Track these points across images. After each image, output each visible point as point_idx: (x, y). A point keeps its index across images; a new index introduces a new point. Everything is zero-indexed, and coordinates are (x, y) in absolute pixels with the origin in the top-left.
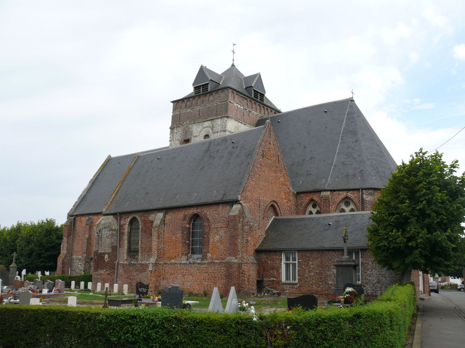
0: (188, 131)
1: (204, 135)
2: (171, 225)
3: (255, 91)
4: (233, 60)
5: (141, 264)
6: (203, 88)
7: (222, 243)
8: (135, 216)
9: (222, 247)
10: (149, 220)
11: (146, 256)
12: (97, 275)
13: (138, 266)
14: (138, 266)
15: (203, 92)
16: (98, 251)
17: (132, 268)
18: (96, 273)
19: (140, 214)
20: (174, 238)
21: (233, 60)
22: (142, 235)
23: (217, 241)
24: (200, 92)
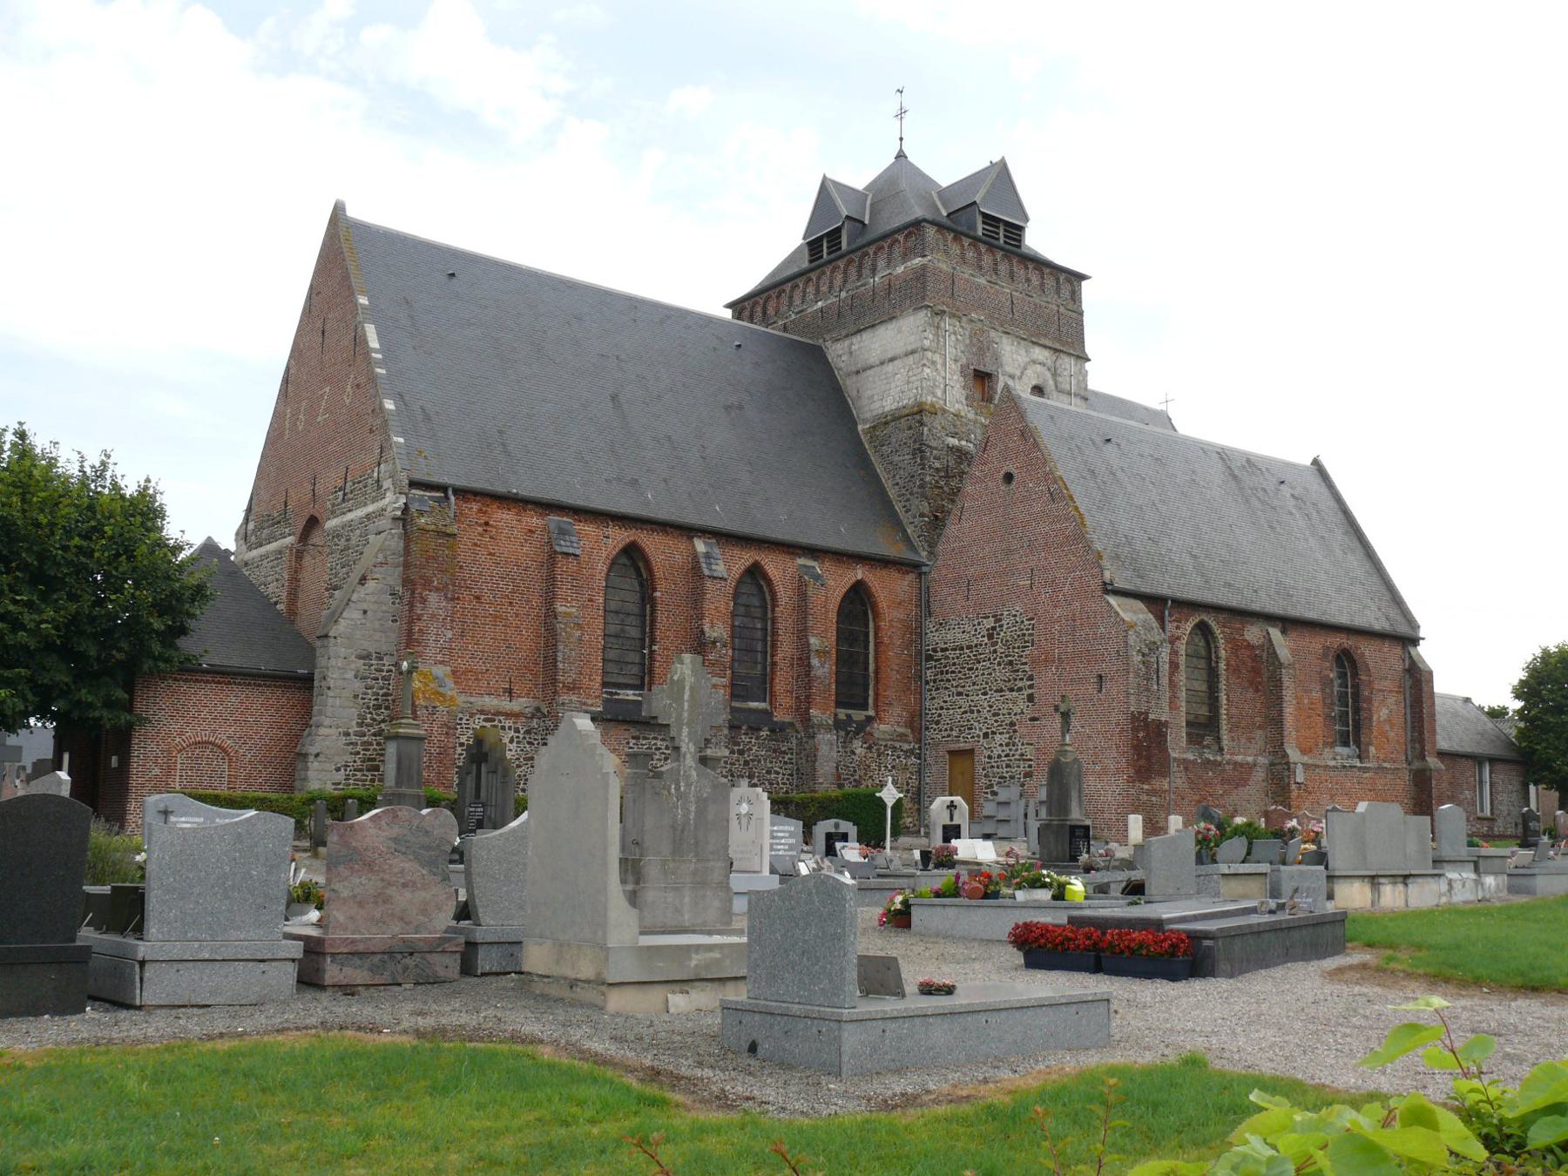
0: (989, 349)
1: (1034, 383)
2: (1297, 666)
3: (985, 216)
4: (901, 139)
5: (1236, 763)
6: (828, 242)
7: (1392, 726)
8: (1206, 619)
9: (1392, 734)
10: (1245, 640)
11: (1243, 741)
12: (1148, 793)
13: (1227, 767)
14: (1227, 767)
15: (829, 254)
16: (1147, 713)
17: (1210, 773)
18: (1146, 787)
19: (1221, 617)
20: (1306, 701)
21: (901, 139)
22: (1227, 680)
23: (1385, 720)
24: (822, 257)
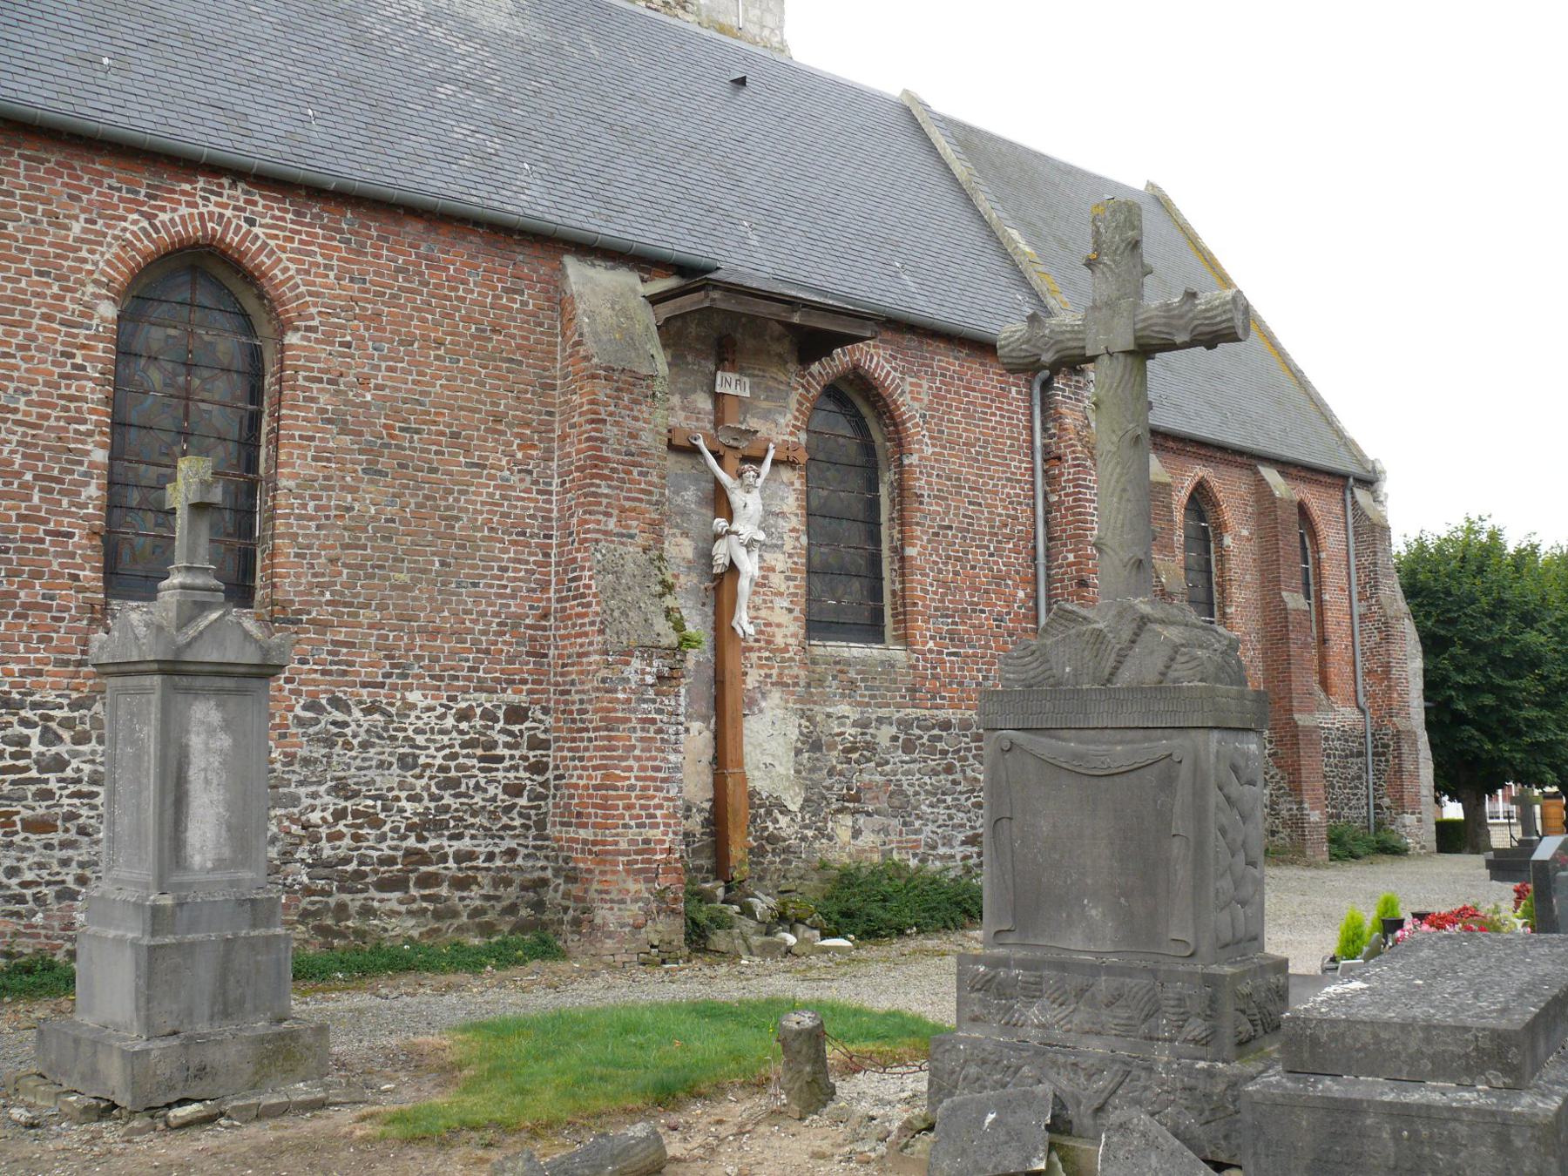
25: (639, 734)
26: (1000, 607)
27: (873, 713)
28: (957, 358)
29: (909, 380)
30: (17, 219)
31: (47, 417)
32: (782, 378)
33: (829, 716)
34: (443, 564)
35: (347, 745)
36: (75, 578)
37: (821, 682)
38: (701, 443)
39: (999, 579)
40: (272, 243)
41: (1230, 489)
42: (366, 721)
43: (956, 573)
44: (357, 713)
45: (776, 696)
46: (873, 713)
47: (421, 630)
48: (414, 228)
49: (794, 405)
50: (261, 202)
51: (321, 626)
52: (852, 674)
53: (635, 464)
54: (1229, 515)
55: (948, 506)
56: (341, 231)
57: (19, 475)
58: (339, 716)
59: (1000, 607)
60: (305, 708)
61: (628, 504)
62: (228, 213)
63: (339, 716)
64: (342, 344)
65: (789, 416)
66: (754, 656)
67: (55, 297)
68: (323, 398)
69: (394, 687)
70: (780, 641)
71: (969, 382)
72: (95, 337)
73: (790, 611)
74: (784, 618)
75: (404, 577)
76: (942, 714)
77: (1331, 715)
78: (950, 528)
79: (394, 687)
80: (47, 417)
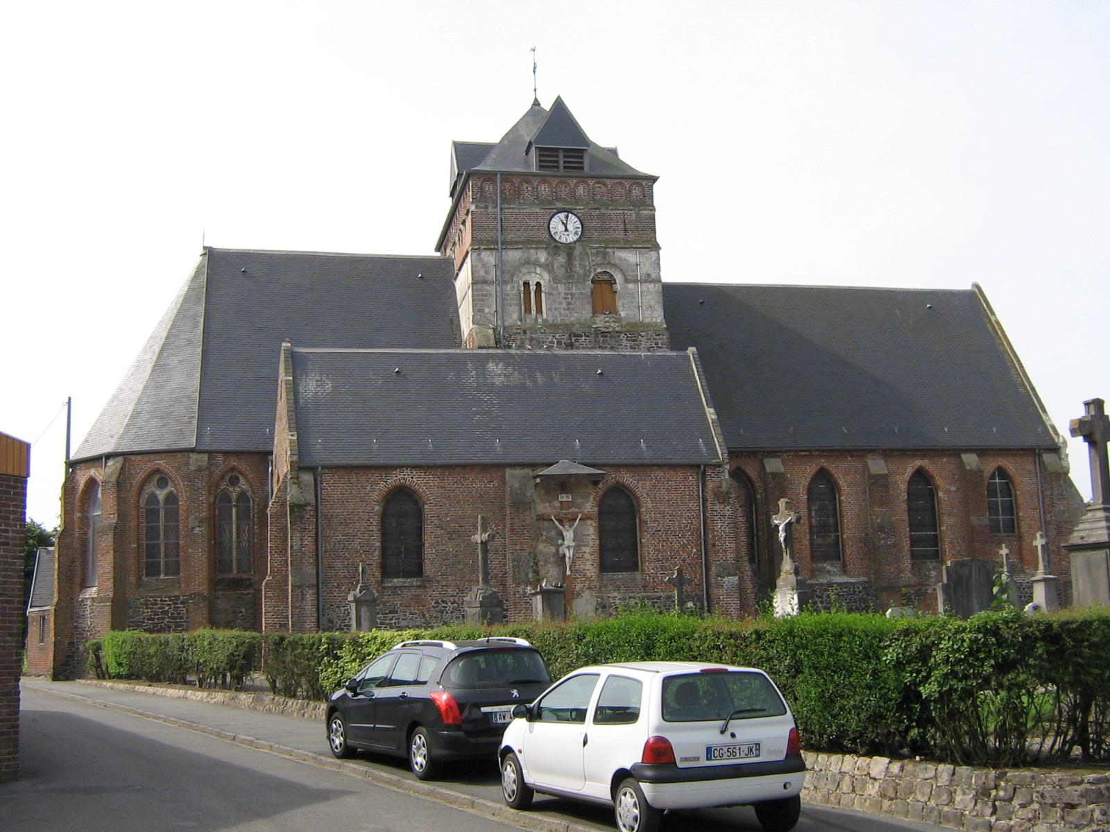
4: (535, 90)
21: (535, 90)
25: (524, 606)
26: (685, 555)
27: (627, 595)
28: (662, 471)
29: (640, 482)
30: (354, 489)
31: (364, 536)
32: (587, 491)
33: (609, 597)
34: (473, 562)
35: (447, 612)
36: (374, 575)
37: (605, 586)
38: (553, 518)
39: (684, 546)
40: (418, 482)
41: (940, 471)
42: (452, 606)
43: (663, 546)
44: (449, 604)
45: (587, 592)
46: (627, 595)
47: (467, 581)
48: (458, 470)
49: (592, 498)
50: (415, 472)
51: (438, 582)
52: (618, 583)
53: (524, 529)
54: (940, 481)
55: (659, 523)
56: (437, 475)
57: (359, 551)
58: (444, 605)
59: (685, 555)
60: (435, 603)
61: (522, 541)
62: (406, 477)
63: (444, 605)
64: (440, 506)
65: (590, 503)
66: (579, 580)
67: (365, 506)
68: (435, 522)
69: (460, 596)
70: (589, 574)
71: (669, 478)
72: (375, 515)
73: (592, 565)
74: (590, 568)
75: (461, 566)
76: (658, 594)
77: (1022, 576)
78: (660, 531)
79: (460, 596)
80: (364, 536)
